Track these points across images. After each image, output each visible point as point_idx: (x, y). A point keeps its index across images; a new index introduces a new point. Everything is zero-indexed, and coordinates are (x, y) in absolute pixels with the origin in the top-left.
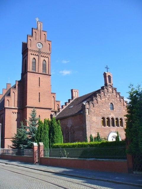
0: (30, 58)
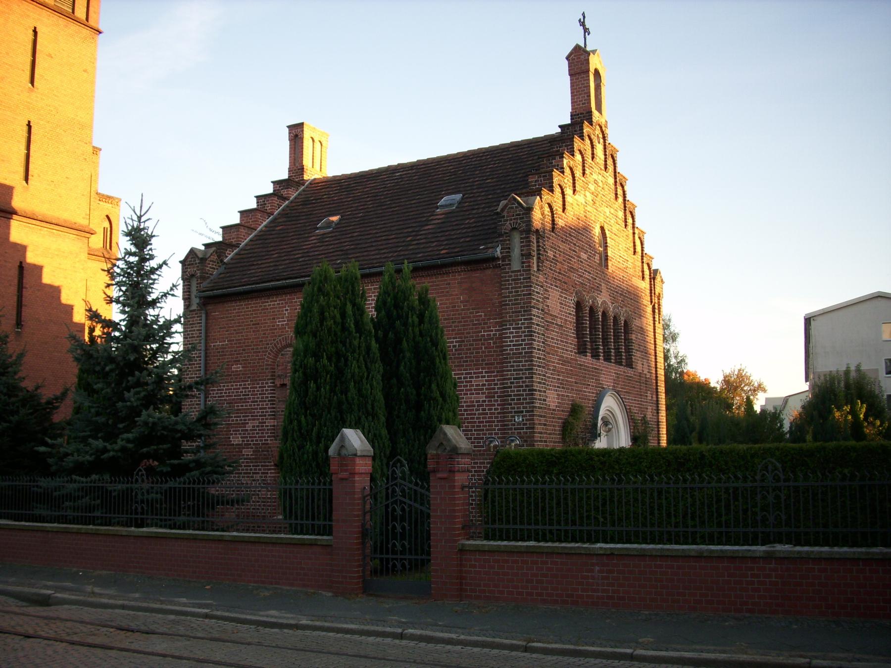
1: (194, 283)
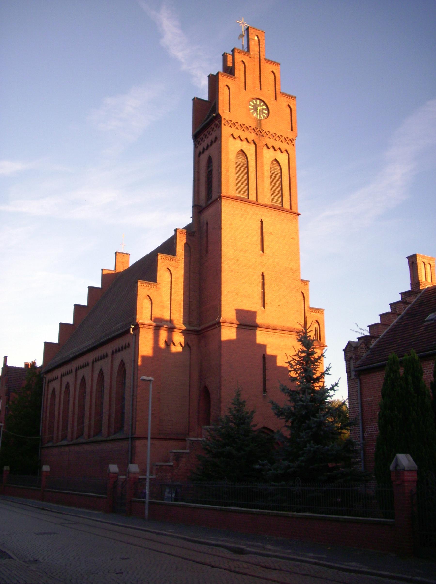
0: (230, 148)
1: (352, 362)
